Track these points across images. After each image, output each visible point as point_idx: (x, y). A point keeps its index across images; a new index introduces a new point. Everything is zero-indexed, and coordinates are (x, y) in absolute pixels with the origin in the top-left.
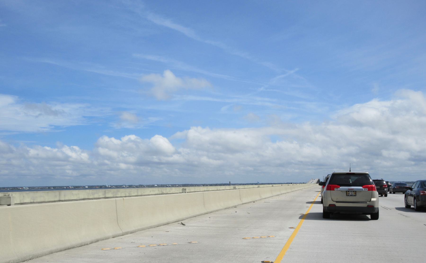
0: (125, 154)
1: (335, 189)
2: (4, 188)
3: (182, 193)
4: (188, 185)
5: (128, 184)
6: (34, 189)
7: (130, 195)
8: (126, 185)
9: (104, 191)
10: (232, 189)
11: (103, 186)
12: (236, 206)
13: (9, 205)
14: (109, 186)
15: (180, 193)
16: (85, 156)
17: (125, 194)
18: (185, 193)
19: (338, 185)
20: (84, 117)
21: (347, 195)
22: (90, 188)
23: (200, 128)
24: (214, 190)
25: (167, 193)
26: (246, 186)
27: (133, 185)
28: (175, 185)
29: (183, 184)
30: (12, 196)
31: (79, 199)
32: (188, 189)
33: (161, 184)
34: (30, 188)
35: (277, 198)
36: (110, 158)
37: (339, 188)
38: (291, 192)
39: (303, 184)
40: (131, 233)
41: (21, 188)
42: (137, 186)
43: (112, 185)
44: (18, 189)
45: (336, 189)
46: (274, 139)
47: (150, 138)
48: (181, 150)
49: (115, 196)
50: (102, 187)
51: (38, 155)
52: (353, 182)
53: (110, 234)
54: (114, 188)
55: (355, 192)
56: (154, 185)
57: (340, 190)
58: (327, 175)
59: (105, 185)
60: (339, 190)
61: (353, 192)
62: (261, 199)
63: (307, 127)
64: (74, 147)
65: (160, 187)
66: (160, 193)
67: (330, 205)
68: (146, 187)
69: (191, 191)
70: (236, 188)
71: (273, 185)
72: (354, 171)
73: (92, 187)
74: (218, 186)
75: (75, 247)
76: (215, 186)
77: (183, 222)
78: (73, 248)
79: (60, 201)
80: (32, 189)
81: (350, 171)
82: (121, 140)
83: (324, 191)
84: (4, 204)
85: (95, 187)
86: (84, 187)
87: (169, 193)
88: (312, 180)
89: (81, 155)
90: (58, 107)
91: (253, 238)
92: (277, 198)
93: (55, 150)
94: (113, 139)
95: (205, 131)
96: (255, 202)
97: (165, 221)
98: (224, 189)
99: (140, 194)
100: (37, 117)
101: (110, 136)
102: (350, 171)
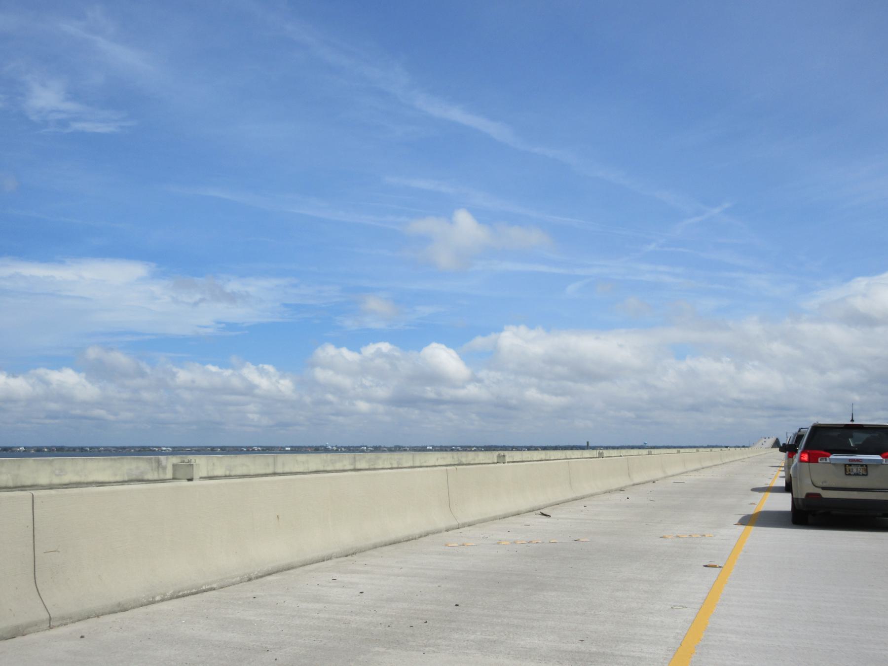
0: (367, 381)
1: (819, 459)
2: (124, 448)
3: (498, 462)
4: (532, 449)
5: (372, 443)
6: (182, 450)
7: (400, 466)
8: (369, 446)
9: (353, 456)
10: (596, 456)
11: (321, 447)
12: (622, 487)
13: (191, 480)
14: (332, 447)
15: (494, 463)
16: (286, 385)
17: (391, 464)
18: (504, 463)
19: (826, 451)
20: (286, 305)
21: (847, 473)
22: (295, 450)
23: (523, 329)
24: (559, 458)
25: (468, 463)
26: (624, 452)
27: (383, 446)
28: (470, 447)
29: (487, 445)
30: (195, 462)
31: (308, 471)
32: (509, 455)
33: (439, 445)
34: (176, 449)
35: (694, 477)
36: (338, 390)
37: (828, 458)
38: (721, 464)
39: (744, 449)
40: (469, 526)
41: (157, 450)
42: (391, 447)
43: (339, 445)
44: (151, 450)
45: (821, 460)
46: (680, 352)
47: (419, 349)
48: (483, 374)
49: (372, 467)
50: (320, 449)
51: (193, 381)
52: (856, 444)
53: (442, 525)
54: (344, 452)
55: (865, 466)
56: (426, 447)
57: (830, 463)
58: (798, 430)
59: (325, 445)
60: (828, 461)
61: (861, 468)
62: (665, 478)
63: (752, 327)
64: (266, 367)
65: (438, 450)
66: (456, 463)
67: (808, 495)
68: (409, 450)
69: (515, 460)
70: (605, 455)
71: (679, 449)
72: (860, 420)
73: (299, 449)
74: (559, 450)
75: (402, 542)
76: (554, 450)
77: (544, 511)
78: (399, 542)
79: (275, 474)
80: (179, 451)
81: (852, 420)
82: (360, 353)
83: (793, 465)
84: (181, 478)
85: (304, 449)
86: (284, 448)
87: (472, 463)
88: (764, 440)
89: (279, 383)
90: (234, 286)
91: (677, 536)
92: (694, 477)
93: (228, 372)
94: (345, 351)
95: (533, 334)
96: (657, 482)
97: (514, 509)
98: (579, 457)
99: (418, 464)
100: (196, 304)
101: (338, 345)
102: (852, 420)
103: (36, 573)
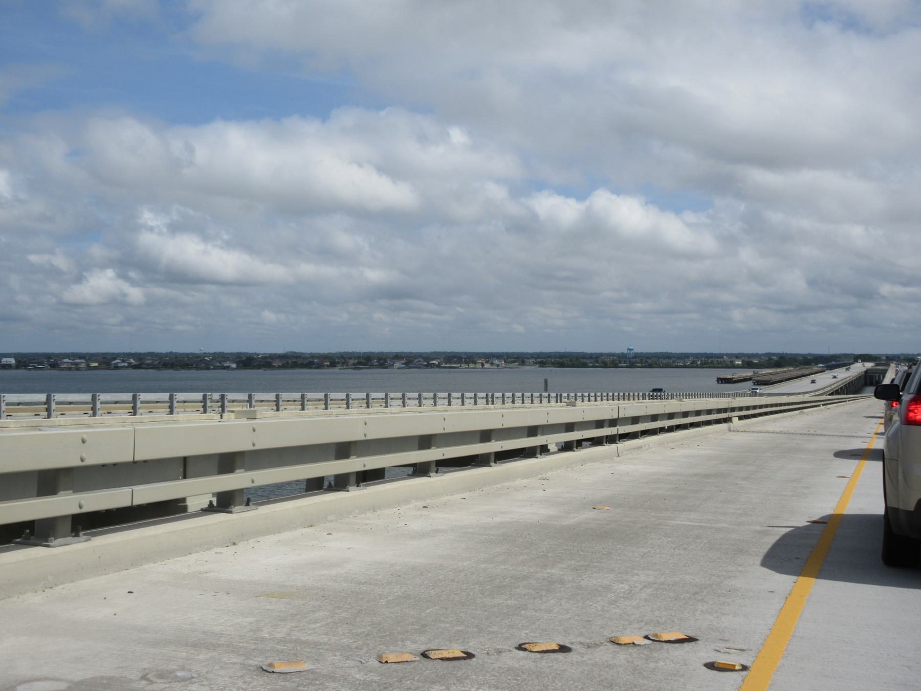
28: (284, 367)
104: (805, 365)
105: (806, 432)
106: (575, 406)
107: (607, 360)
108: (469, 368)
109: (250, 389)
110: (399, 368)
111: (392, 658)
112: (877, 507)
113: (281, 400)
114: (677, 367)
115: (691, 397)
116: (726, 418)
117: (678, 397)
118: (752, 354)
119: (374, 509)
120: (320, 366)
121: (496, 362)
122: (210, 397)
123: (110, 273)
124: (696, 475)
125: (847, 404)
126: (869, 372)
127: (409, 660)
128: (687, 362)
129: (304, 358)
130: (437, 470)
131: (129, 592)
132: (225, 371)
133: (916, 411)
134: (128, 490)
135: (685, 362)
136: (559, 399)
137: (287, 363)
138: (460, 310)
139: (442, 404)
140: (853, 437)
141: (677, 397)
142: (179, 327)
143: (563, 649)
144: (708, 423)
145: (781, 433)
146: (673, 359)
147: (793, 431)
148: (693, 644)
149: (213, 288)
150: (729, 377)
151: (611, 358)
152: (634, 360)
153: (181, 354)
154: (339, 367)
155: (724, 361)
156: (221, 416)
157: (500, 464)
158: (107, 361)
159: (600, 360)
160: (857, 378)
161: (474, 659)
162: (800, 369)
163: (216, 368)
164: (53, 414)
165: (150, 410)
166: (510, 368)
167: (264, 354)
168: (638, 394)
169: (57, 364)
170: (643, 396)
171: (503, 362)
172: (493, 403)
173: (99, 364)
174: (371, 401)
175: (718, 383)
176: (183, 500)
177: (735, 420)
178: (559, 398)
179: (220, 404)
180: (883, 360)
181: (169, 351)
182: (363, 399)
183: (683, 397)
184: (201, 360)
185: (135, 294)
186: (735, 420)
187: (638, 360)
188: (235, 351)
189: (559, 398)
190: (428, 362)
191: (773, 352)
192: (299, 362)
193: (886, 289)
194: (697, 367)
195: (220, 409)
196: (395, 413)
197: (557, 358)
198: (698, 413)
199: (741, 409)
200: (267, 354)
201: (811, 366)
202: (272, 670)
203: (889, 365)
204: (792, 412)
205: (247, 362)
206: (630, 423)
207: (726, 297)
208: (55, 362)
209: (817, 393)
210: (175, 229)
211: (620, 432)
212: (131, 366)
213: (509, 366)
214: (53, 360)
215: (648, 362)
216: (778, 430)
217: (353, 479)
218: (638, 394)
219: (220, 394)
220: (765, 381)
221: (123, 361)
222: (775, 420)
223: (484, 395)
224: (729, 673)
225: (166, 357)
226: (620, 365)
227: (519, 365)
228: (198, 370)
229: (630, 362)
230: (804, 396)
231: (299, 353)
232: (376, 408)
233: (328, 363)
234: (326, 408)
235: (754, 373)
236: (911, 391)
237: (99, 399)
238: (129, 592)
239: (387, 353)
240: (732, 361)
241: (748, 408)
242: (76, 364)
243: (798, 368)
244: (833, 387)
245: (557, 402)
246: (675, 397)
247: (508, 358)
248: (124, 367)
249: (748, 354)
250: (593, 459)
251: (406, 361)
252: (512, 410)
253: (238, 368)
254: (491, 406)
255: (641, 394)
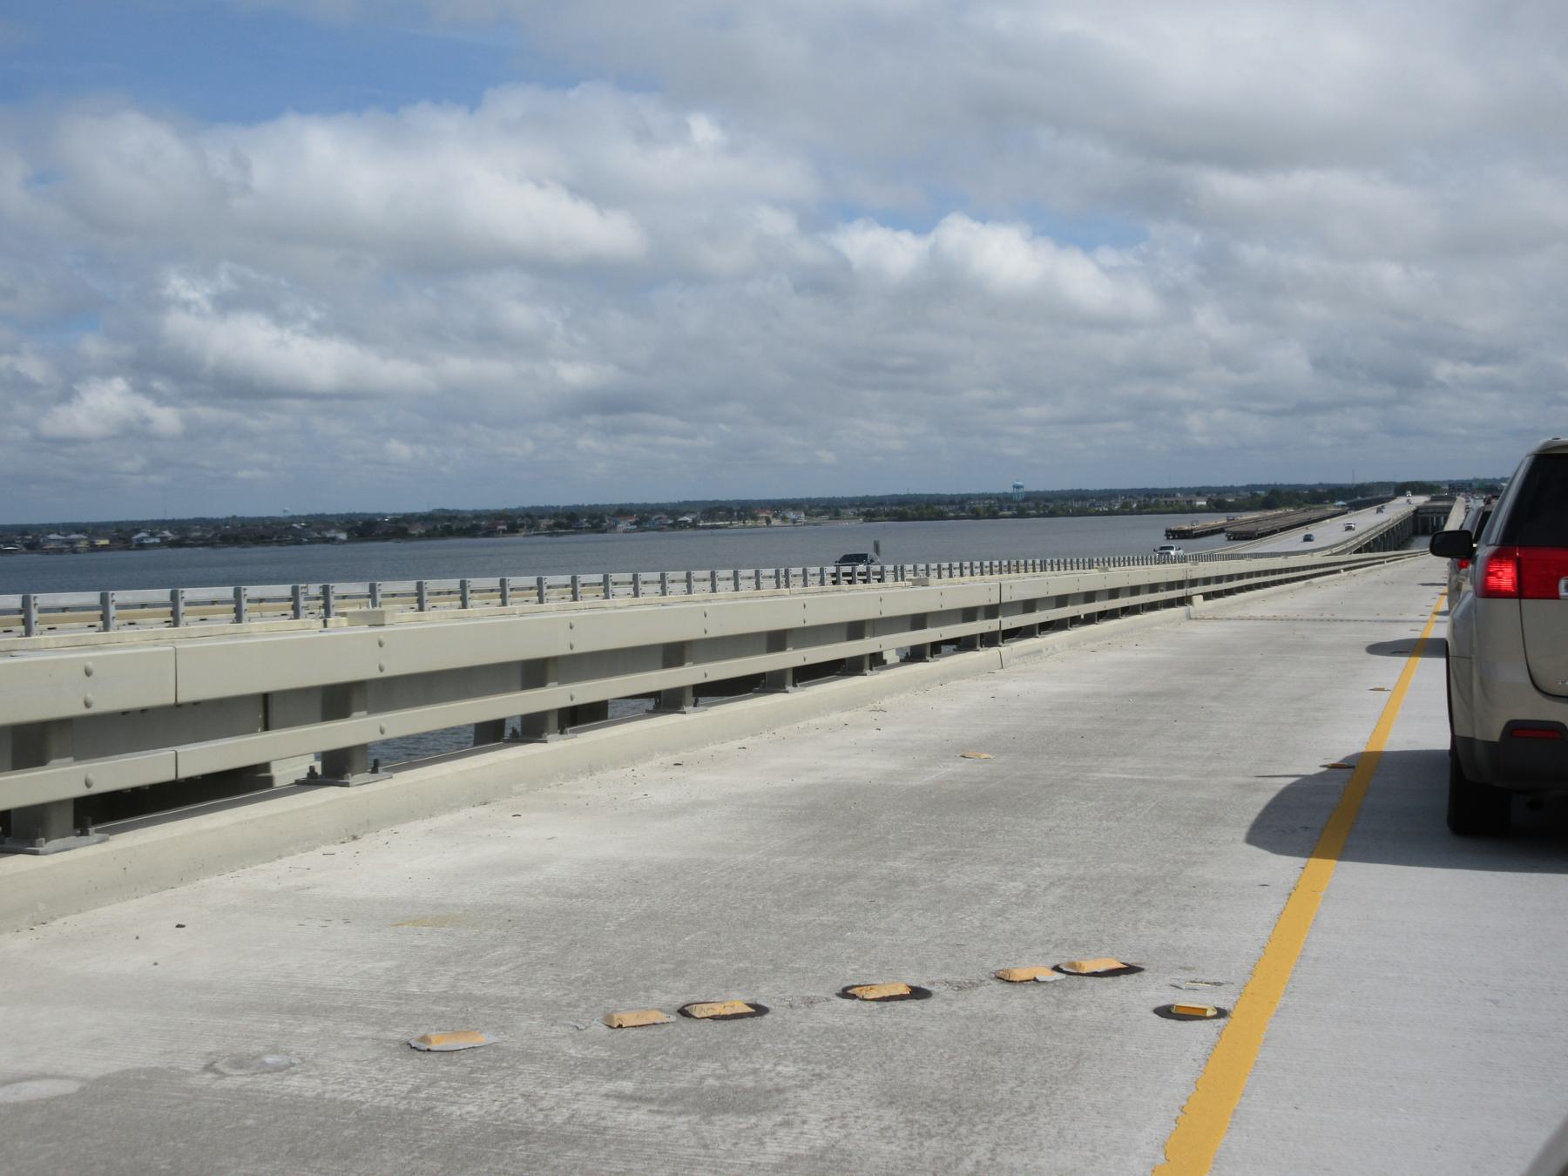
28: (429, 535)
67: (1515, 729)
103: (178, 656)
104: (1313, 504)
105: (1315, 617)
106: (927, 585)
107: (979, 506)
108: (744, 527)
109: (372, 576)
110: (626, 532)
111: (629, 1019)
112: (1438, 738)
113: (425, 592)
114: (1098, 514)
115: (1149, 563)
116: (1183, 598)
117: (1102, 564)
118: (1225, 487)
119: (591, 770)
120: (490, 532)
121: (792, 515)
122: (304, 590)
123: (119, 384)
124: (1136, 694)
125: (1384, 567)
126: (1420, 511)
127: (658, 1021)
128: (1115, 506)
129: (464, 519)
130: (697, 701)
131: (178, 926)
132: (329, 546)
133: (1500, 574)
134: (167, 753)
135: (1110, 504)
136: (899, 574)
137: (435, 529)
138: (722, 427)
139: (701, 589)
140: (1397, 621)
141: (1098, 565)
142: (244, 474)
143: (918, 993)
144: (1153, 607)
145: (1275, 619)
146: (1091, 500)
147: (1295, 616)
148: (1134, 976)
149: (299, 404)
150: (1186, 528)
151: (987, 502)
152: (1026, 504)
153: (252, 520)
154: (523, 534)
155: (1177, 501)
156: (325, 622)
157: (877, 672)
158: (124, 536)
159: (967, 507)
160: (1400, 523)
161: (767, 1017)
162: (1305, 511)
163: (312, 541)
164: (35, 628)
165: (284, 613)
166: (815, 524)
167: (394, 514)
168: (1034, 562)
169: (38, 542)
170: (1041, 565)
171: (803, 515)
172: (787, 586)
173: (111, 542)
174: (579, 589)
175: (1168, 539)
176: (265, 767)
177: (1198, 600)
178: (899, 573)
179: (321, 602)
180: (1444, 491)
181: (230, 515)
182: (567, 586)
183: (1109, 565)
184: (286, 529)
185: (166, 419)
186: (1198, 600)
187: (1032, 504)
188: (344, 511)
189: (899, 573)
190: (675, 520)
191: (1259, 483)
192: (454, 527)
193: (1444, 370)
194: (1132, 513)
195: (323, 610)
196: (621, 608)
197: (896, 505)
198: (1135, 590)
199: (1207, 581)
200: (399, 514)
201: (1321, 506)
202: (427, 1047)
203: (1454, 499)
204: (1281, 587)
205: (365, 529)
206: (1054, 604)
207: (1176, 392)
208: (35, 541)
209: (1335, 550)
210: (225, 304)
211: (1004, 627)
212: (167, 543)
213: (811, 522)
214: (30, 537)
215: (1048, 507)
216: (1270, 614)
217: (553, 721)
218: (1026, 563)
219: (321, 585)
220: (1247, 533)
221: (152, 535)
222: (1264, 599)
223: (771, 572)
224: (1196, 1023)
225: (226, 525)
226: (1001, 513)
227: (830, 519)
228: (267, 546)
229: (1018, 508)
230: (1312, 556)
231: (454, 510)
232: (589, 600)
233: (505, 527)
234: (504, 604)
235: (1228, 520)
236: (1492, 540)
237: (113, 601)
238: (178, 926)
239: (603, 506)
240: (1191, 501)
241: (1219, 579)
242: (72, 542)
243: (1302, 509)
244: (1360, 538)
245: (896, 580)
246: (1095, 565)
247: (811, 508)
248: (154, 545)
249: (1217, 488)
250: (960, 675)
251: (638, 519)
252: (820, 596)
253: (350, 540)
254: (784, 590)
255: (1038, 561)
